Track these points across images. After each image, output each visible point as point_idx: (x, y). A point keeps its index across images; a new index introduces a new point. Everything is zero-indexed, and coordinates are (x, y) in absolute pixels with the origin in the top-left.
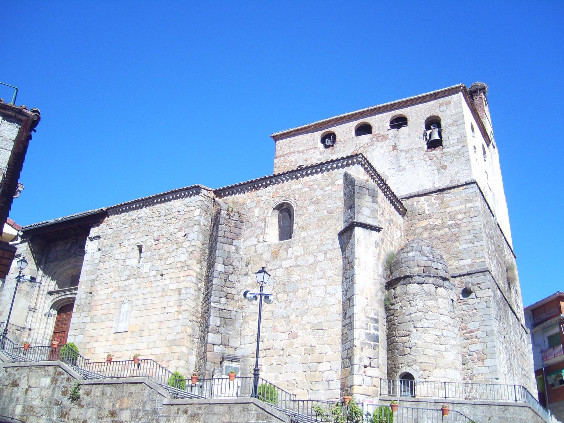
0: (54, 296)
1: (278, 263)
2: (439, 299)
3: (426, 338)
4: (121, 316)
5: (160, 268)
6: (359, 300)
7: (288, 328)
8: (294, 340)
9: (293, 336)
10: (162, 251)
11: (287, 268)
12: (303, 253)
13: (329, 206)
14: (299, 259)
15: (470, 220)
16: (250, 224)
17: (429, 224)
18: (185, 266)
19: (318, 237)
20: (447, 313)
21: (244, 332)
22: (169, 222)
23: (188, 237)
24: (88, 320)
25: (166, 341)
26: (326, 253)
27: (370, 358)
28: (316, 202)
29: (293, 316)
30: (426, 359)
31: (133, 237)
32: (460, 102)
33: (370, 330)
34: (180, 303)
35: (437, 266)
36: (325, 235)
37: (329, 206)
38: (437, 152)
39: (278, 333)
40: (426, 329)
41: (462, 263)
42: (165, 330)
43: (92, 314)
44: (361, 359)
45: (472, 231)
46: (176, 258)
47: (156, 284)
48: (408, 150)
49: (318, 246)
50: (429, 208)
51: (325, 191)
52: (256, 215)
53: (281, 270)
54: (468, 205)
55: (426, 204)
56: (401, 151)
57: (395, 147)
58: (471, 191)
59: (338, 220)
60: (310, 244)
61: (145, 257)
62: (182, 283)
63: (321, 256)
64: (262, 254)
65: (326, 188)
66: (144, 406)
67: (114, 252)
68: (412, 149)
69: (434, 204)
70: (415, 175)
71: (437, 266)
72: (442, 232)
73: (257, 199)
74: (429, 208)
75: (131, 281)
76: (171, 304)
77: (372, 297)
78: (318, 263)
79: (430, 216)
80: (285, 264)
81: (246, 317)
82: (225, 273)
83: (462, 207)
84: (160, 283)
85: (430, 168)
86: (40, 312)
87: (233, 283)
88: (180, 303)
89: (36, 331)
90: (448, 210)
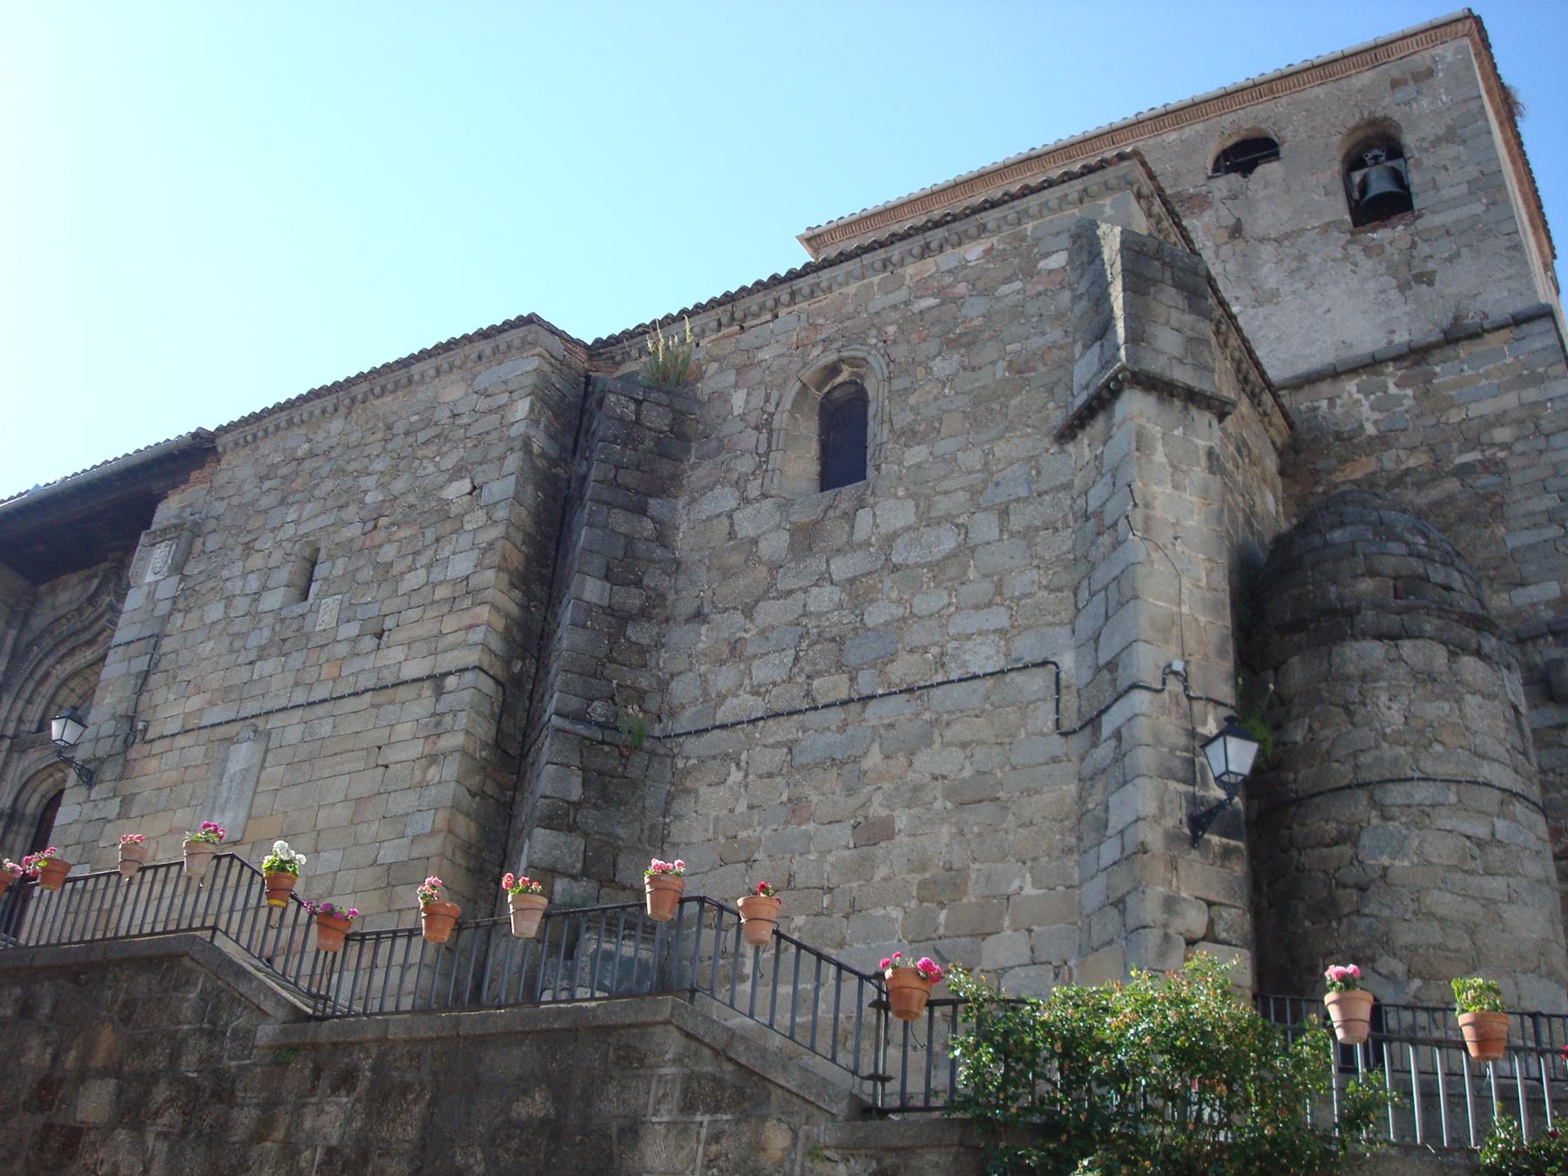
1: (815, 564)
2: (1468, 697)
3: (1427, 848)
4: (225, 787)
5: (374, 610)
7: (854, 802)
8: (879, 851)
9: (873, 833)
10: (388, 553)
11: (852, 581)
12: (912, 519)
13: (1016, 346)
14: (899, 544)
15: (1541, 443)
16: (714, 444)
17: (1382, 470)
18: (467, 590)
19: (973, 459)
20: (1505, 756)
21: (677, 831)
22: (420, 453)
23: (485, 492)
24: (114, 807)
25: (375, 869)
26: (1004, 513)
27: (1210, 904)
28: (967, 341)
29: (874, 759)
30: (1433, 933)
31: (292, 516)
32: (1469, 67)
33: (1205, 785)
34: (438, 724)
35: (1448, 575)
36: (1000, 449)
37: (1016, 346)
38: (1390, 235)
39: (811, 826)
40: (1425, 813)
41: (1523, 597)
42: (375, 827)
43: (127, 788)
44: (1170, 904)
45: (1553, 483)
46: (435, 570)
47: (357, 665)
48: (1287, 236)
49: (975, 492)
50: (1377, 416)
51: (998, 299)
52: (738, 411)
53: (828, 588)
54: (1531, 395)
55: (1366, 403)
56: (1261, 241)
57: (1236, 231)
58: (1537, 345)
59: (1051, 392)
60: (944, 485)
61: (325, 579)
62: (450, 655)
63: (985, 527)
64: (754, 542)
65: (1005, 289)
66: (175, 1056)
67: (225, 573)
68: (1301, 232)
69: (1398, 400)
70: (1319, 311)
71: (1448, 575)
72: (1434, 493)
73: (738, 360)
74: (1377, 416)
75: (268, 666)
76: (405, 730)
77: (1206, 657)
78: (973, 550)
79: (1383, 441)
80: (841, 568)
81: (687, 772)
82: (610, 611)
83: (1509, 400)
84: (368, 663)
85: (1372, 285)
87: (642, 650)
88: (438, 724)
90: (1455, 416)
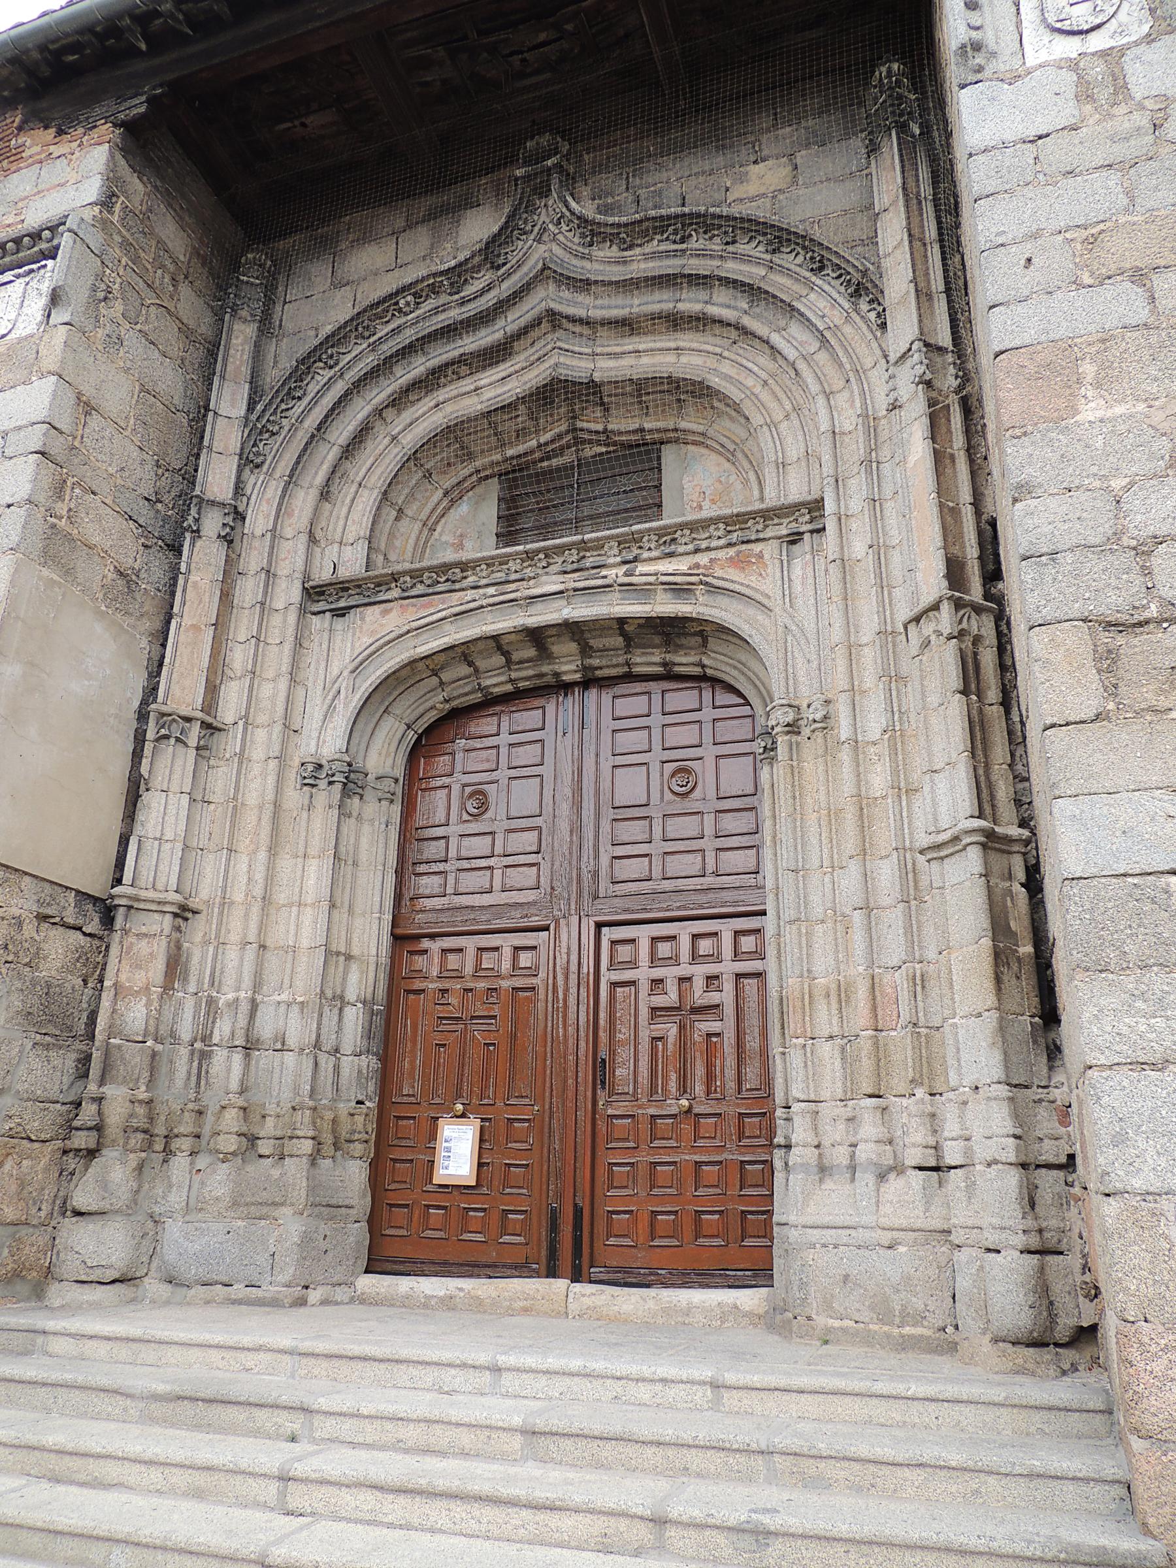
0: (376, 623)
6: (897, 1530)
86: (257, 753)
89: (235, 927)
